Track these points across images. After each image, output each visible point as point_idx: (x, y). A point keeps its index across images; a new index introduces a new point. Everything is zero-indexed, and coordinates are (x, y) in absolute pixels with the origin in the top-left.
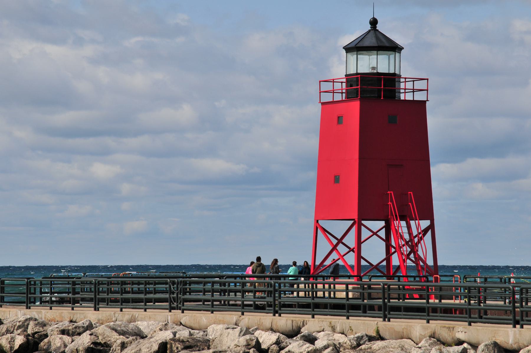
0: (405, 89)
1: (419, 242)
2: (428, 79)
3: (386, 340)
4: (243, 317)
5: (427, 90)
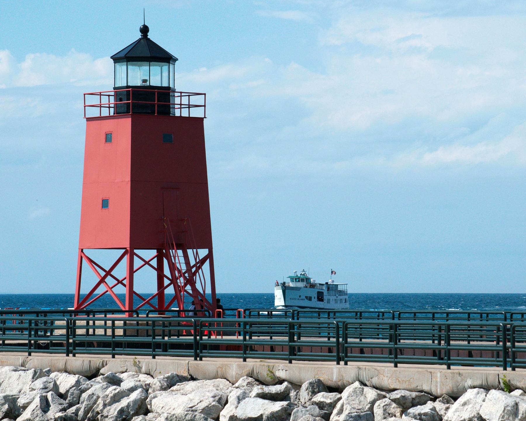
0: (181, 104)
1: (197, 271)
2: (205, 94)
3: (198, 380)
4: (30, 357)
5: (205, 106)
